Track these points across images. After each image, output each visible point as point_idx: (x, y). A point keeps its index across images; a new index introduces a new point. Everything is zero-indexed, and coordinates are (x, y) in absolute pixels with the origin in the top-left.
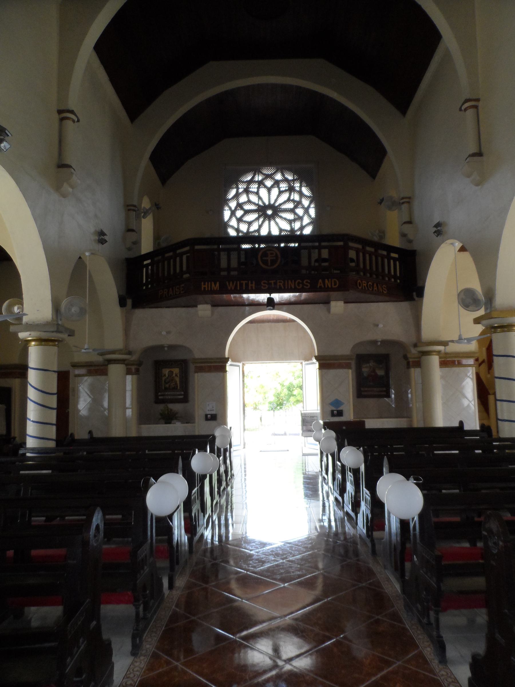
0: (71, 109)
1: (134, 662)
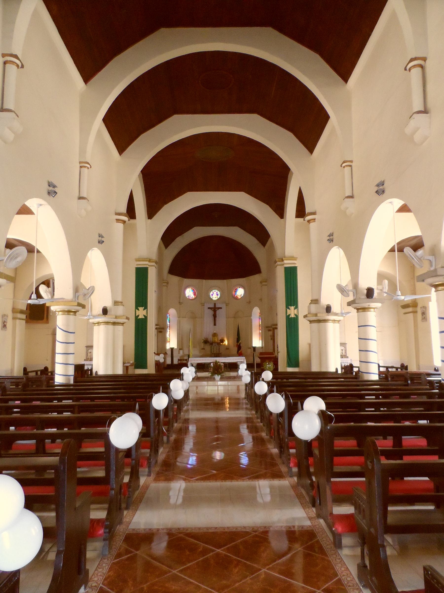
0: (14, 53)
1: (98, 568)
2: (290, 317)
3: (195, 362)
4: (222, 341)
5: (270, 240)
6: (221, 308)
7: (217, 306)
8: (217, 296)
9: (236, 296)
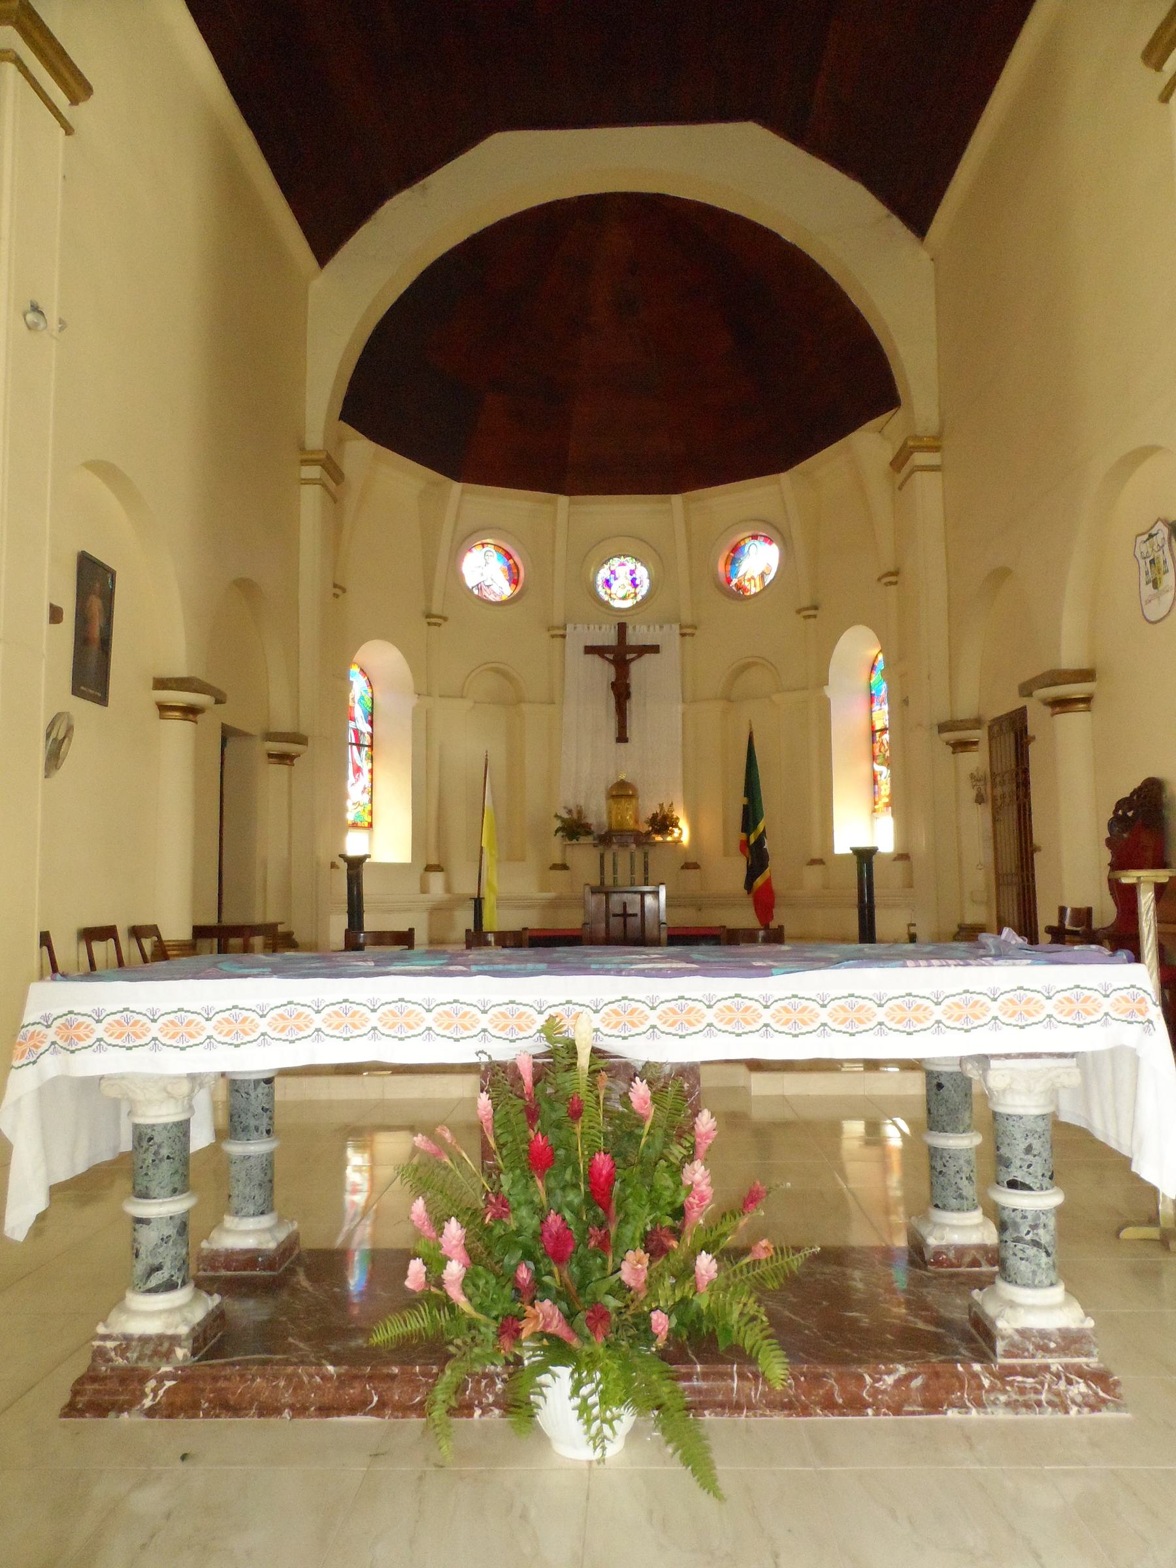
3: (178, 1063)
4: (663, 823)
6: (655, 649)
7: (633, 639)
8: (633, 590)
9: (735, 581)
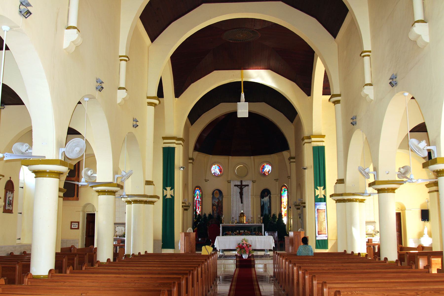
2: (170, 188)
5: (297, 115)
6: (248, 185)
7: (244, 183)
